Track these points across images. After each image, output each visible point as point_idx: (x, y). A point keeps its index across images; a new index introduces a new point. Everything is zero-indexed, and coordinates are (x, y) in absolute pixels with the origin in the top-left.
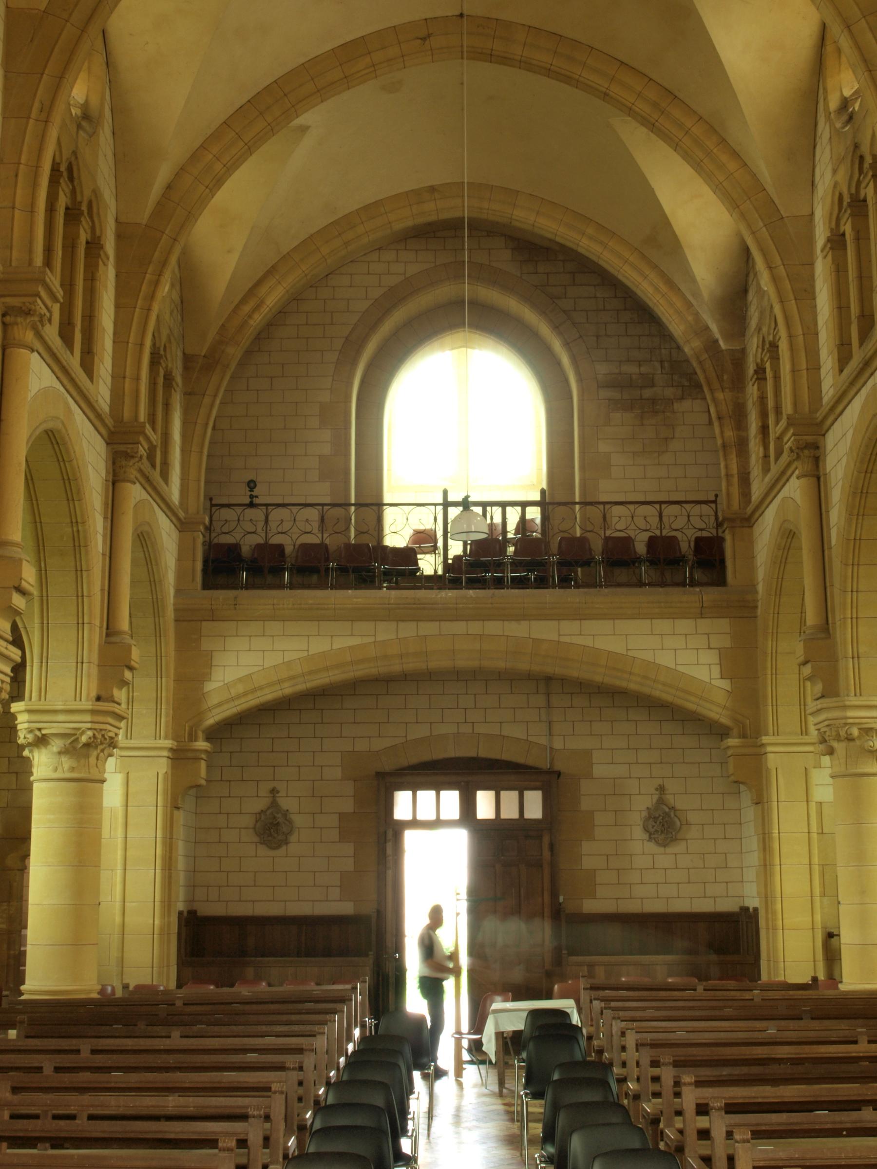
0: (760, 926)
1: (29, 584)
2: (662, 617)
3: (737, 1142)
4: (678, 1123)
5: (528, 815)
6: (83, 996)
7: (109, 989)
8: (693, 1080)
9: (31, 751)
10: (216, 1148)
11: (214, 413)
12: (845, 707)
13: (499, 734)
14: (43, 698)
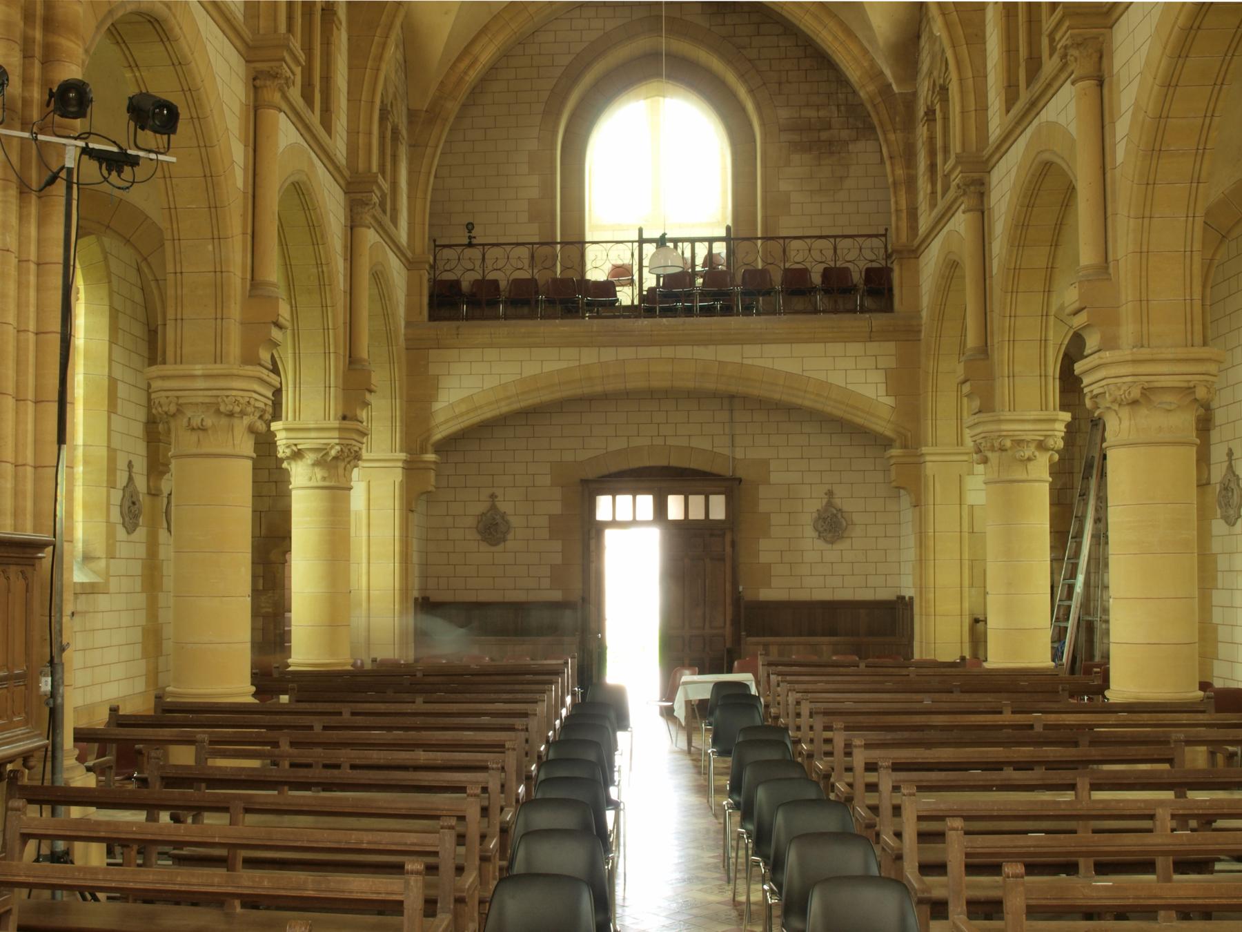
0: (915, 612)
1: (286, 320)
2: (834, 340)
3: (904, 795)
4: (848, 777)
5: (712, 517)
6: (339, 668)
7: (359, 662)
8: (863, 743)
9: (289, 464)
10: (466, 793)
11: (436, 162)
12: (1000, 421)
13: (687, 445)
14: (297, 419)
